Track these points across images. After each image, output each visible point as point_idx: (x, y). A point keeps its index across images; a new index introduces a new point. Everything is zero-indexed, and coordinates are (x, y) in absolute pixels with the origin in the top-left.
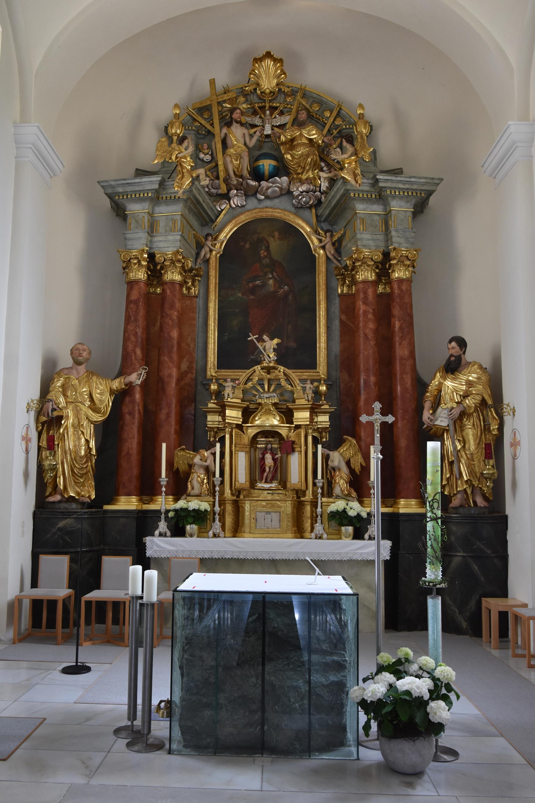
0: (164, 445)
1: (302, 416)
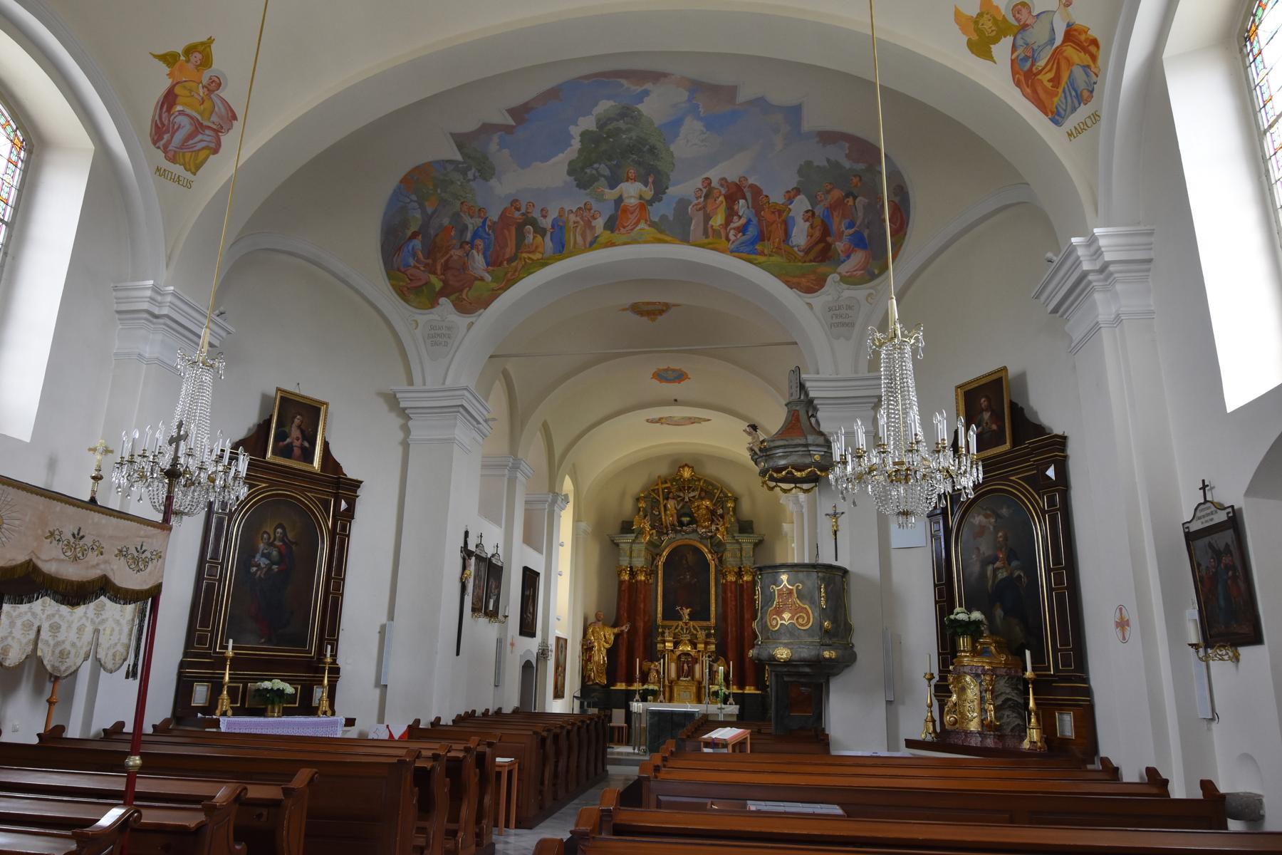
1: (701, 646)
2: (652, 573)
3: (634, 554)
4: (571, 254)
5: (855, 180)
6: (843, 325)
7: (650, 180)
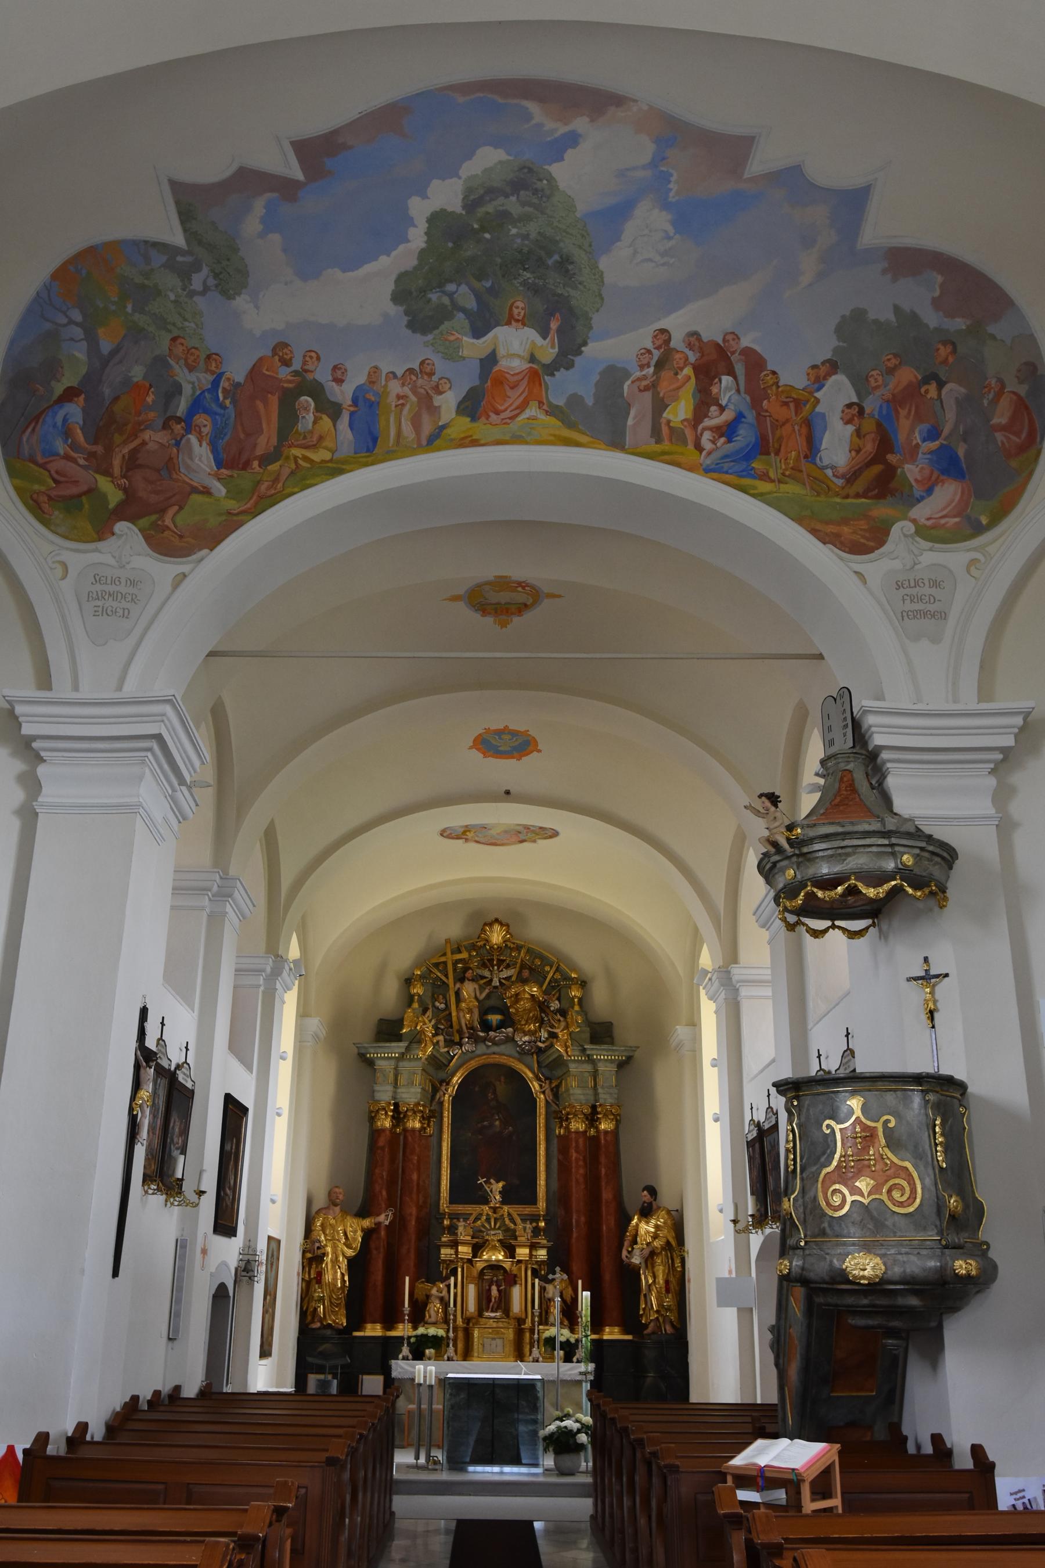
0: (407, 1279)
1: (522, 1252)
2: (433, 1115)
3: (402, 1080)
4: (390, 455)
5: (944, 351)
6: (925, 614)
7: (554, 325)
